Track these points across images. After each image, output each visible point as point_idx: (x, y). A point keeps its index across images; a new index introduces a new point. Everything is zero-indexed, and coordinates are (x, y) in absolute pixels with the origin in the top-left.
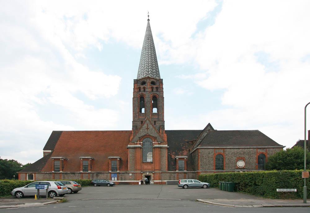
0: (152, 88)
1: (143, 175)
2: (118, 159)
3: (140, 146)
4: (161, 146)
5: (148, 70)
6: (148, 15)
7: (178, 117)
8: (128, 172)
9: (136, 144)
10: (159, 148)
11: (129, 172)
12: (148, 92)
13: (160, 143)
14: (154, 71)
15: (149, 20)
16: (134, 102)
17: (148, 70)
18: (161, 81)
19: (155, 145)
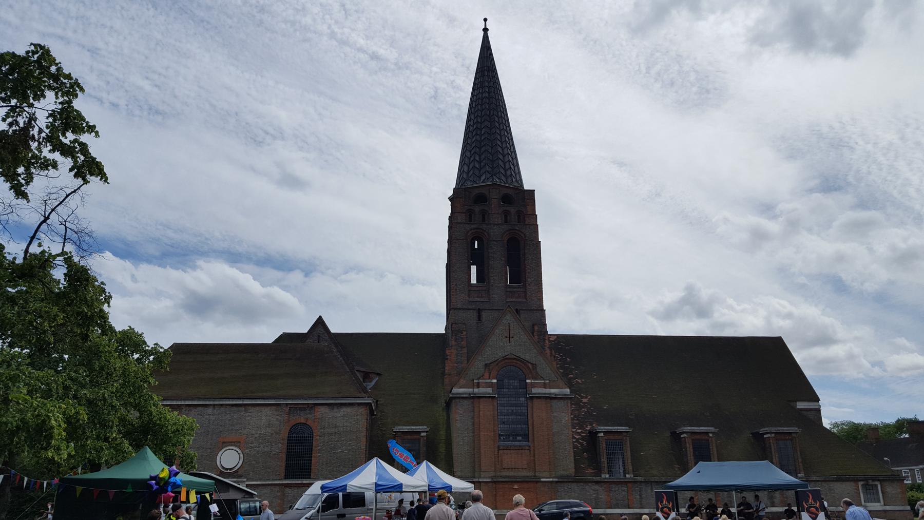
3: (489, 390)
9: (478, 386)
15: (486, 30)
19: (534, 390)
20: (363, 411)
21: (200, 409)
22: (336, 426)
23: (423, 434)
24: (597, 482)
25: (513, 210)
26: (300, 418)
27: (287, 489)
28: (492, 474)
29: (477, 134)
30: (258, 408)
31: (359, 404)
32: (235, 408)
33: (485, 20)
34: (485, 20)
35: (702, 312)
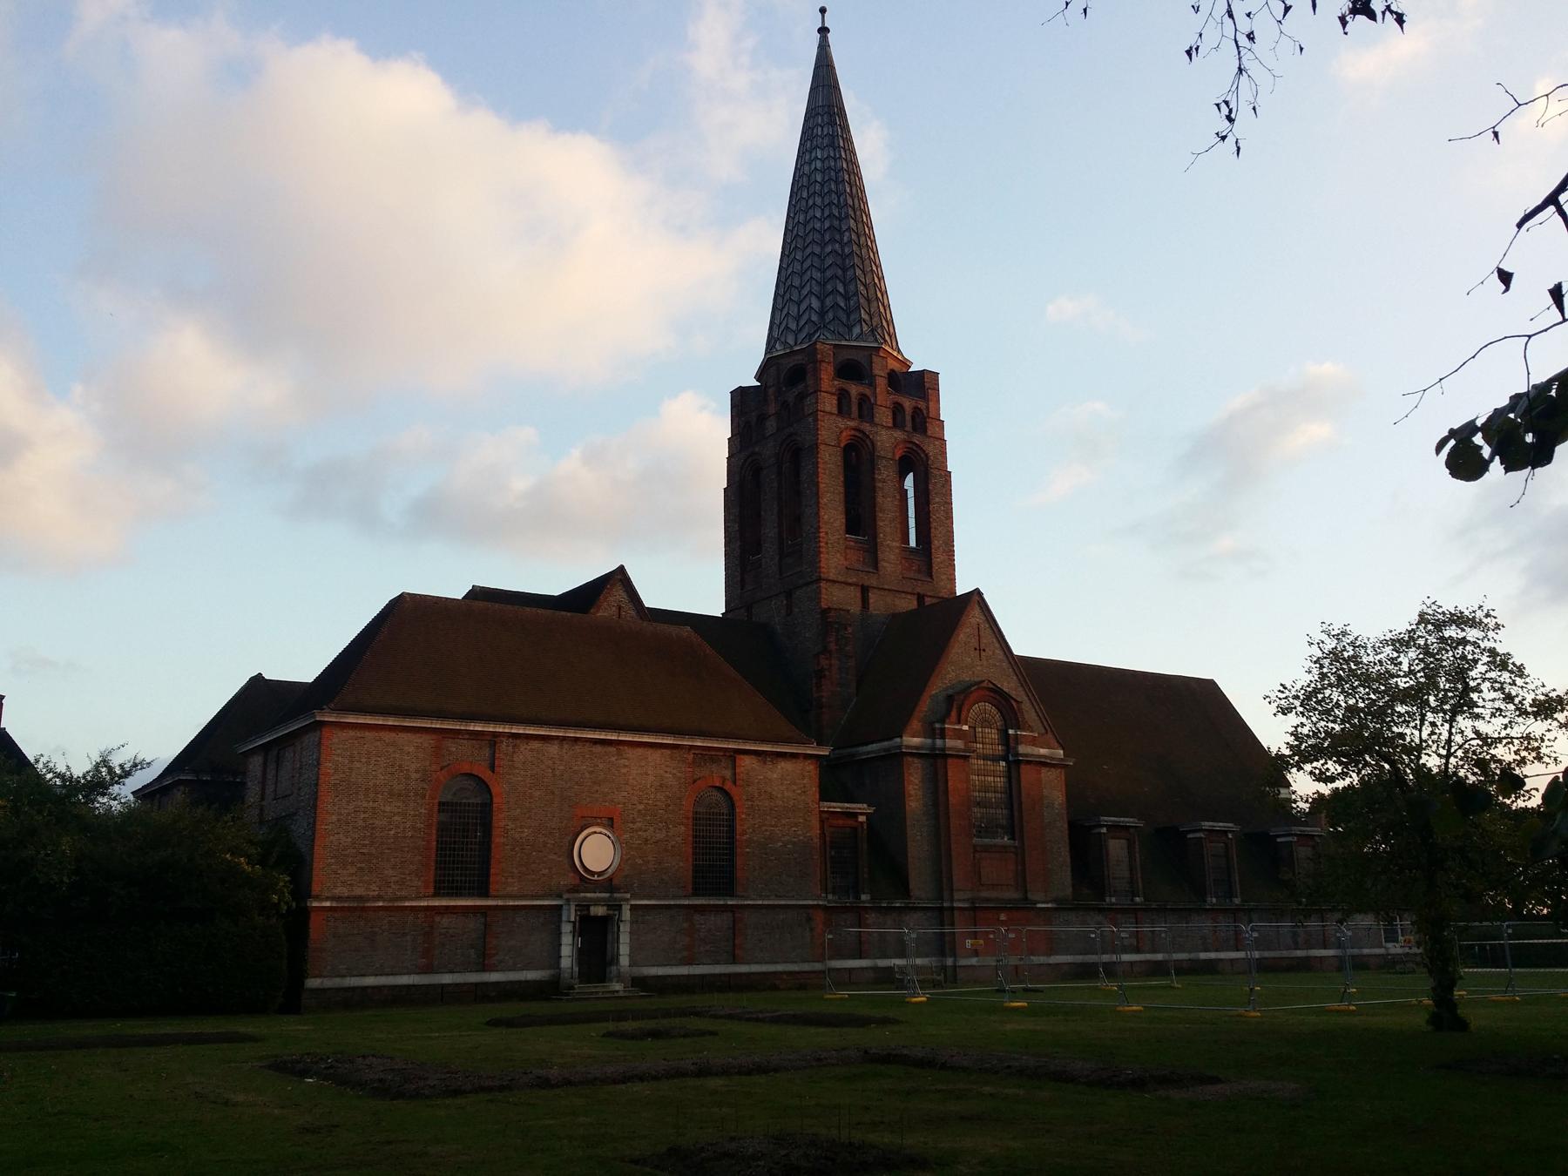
3: (959, 744)
12: (834, 420)
15: (823, 31)
18: (923, 385)
20: (811, 768)
21: (536, 745)
22: (771, 797)
23: (862, 819)
24: (1101, 910)
25: (908, 404)
26: (718, 773)
27: (697, 917)
28: (968, 895)
29: (833, 240)
30: (640, 751)
31: (807, 756)
32: (598, 749)
33: (823, 11)
34: (823, 11)
35: (434, 516)
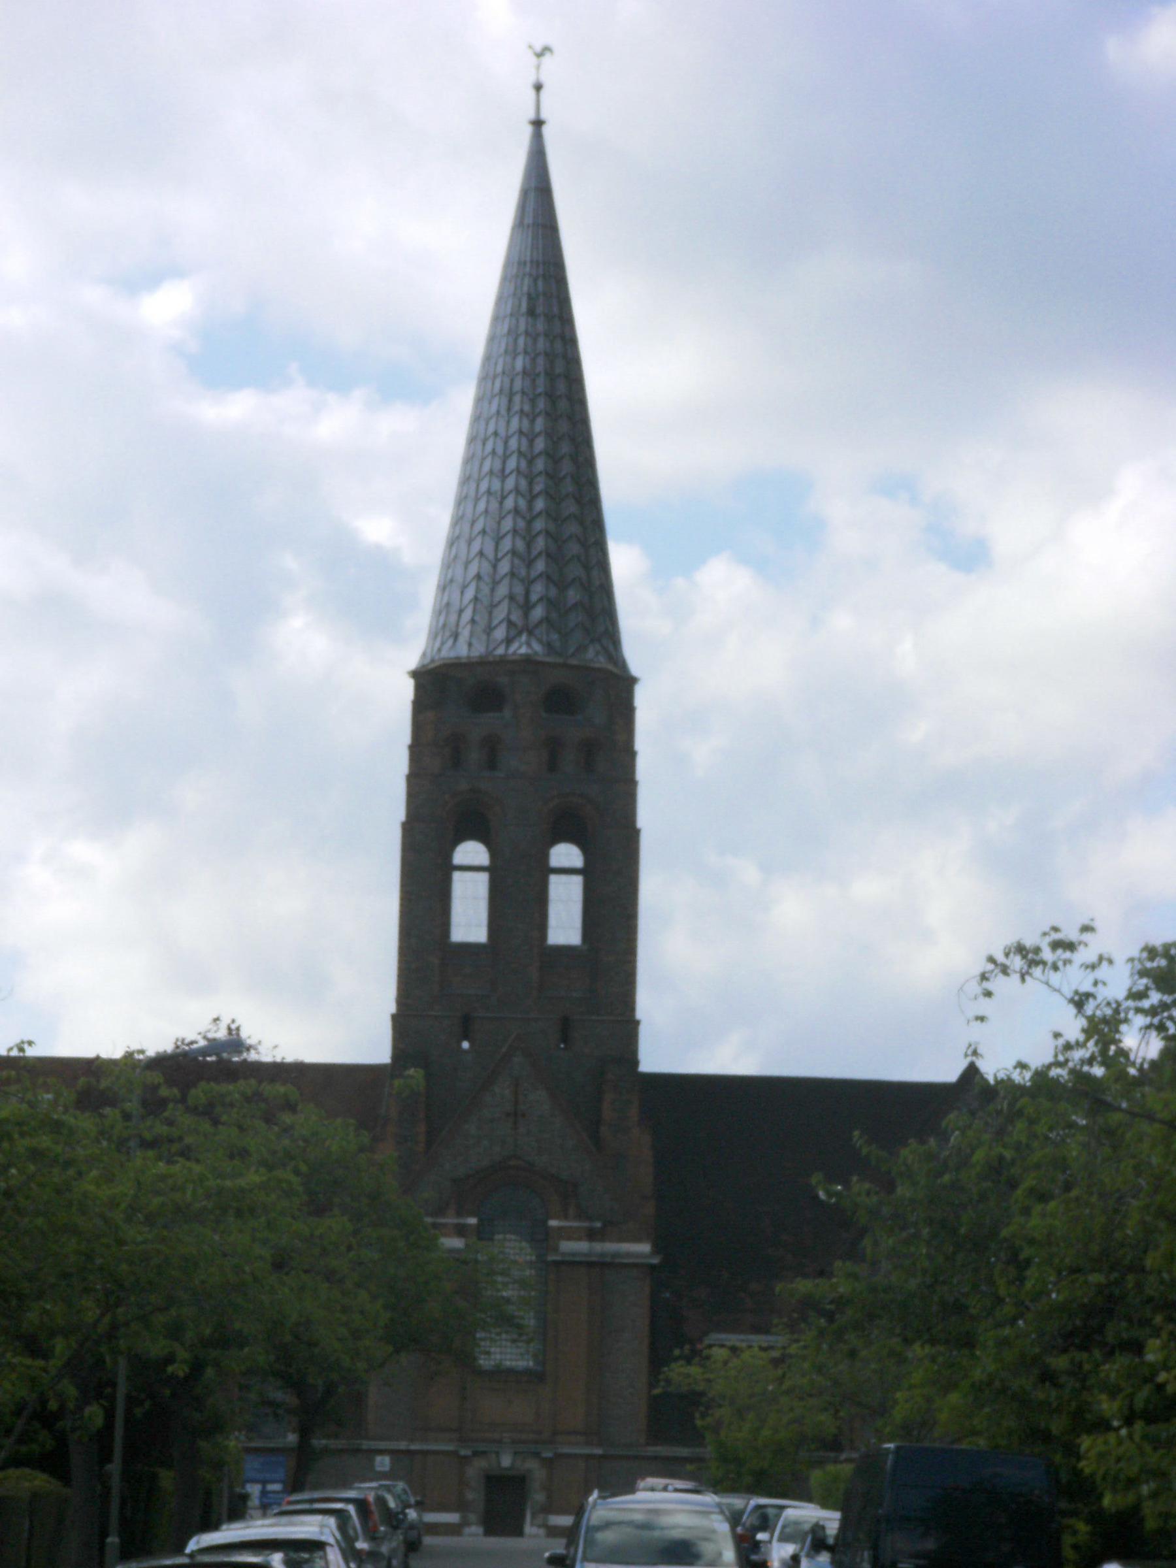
0: (553, 748)
1: (475, 1470)
2: (469, 916)
4: (610, 1247)
5: (527, 593)
6: (532, 79)
7: (777, 949)
8: (366, 1444)
10: (590, 1265)
11: (373, 1445)
12: (526, 733)
13: (598, 1225)
14: (573, 595)
15: (538, 124)
16: (593, 656)
17: (527, 593)
